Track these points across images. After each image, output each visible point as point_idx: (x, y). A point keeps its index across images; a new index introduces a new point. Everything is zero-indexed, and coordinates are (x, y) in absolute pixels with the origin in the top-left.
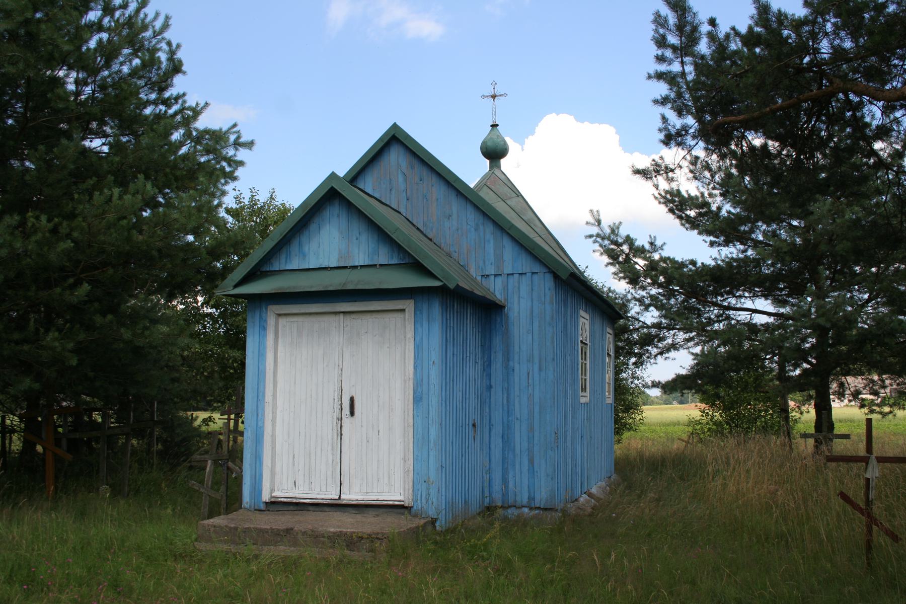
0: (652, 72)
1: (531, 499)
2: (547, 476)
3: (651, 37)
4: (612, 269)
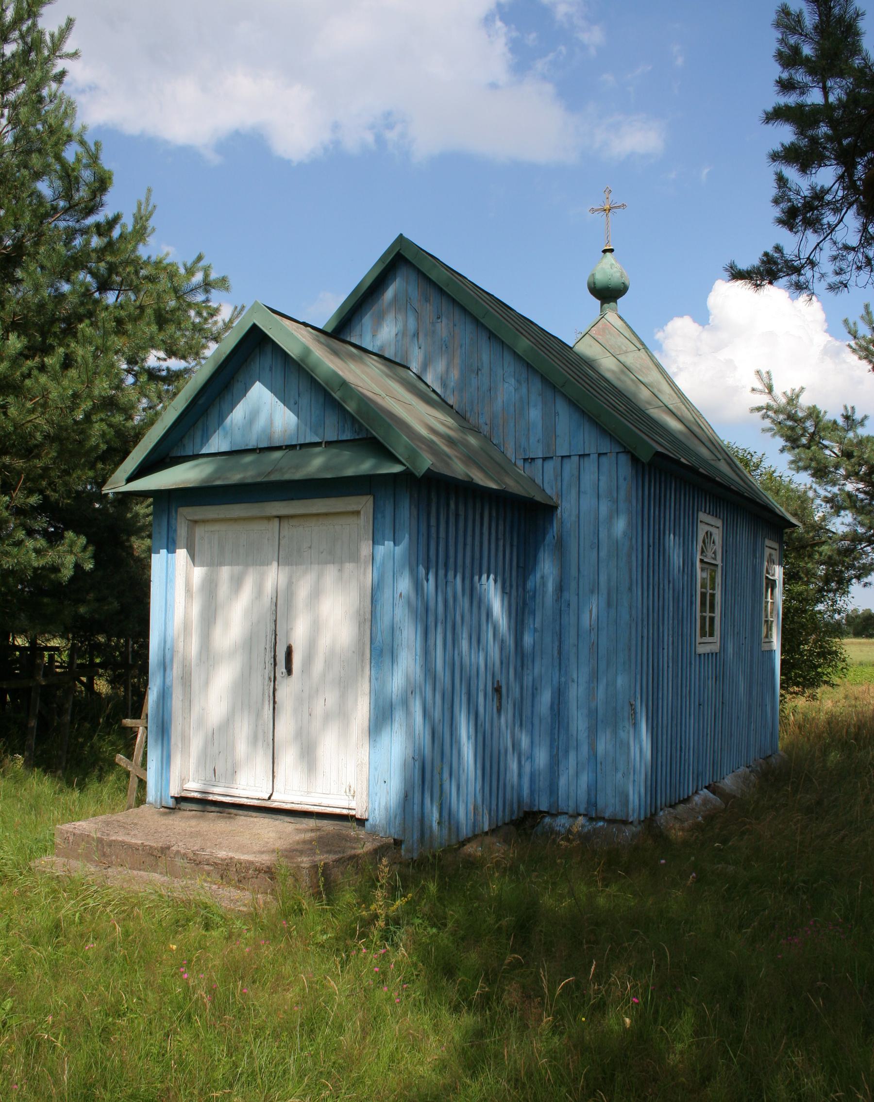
0: (770, 109)
1: (592, 803)
3: (773, 52)
4: (788, 456)
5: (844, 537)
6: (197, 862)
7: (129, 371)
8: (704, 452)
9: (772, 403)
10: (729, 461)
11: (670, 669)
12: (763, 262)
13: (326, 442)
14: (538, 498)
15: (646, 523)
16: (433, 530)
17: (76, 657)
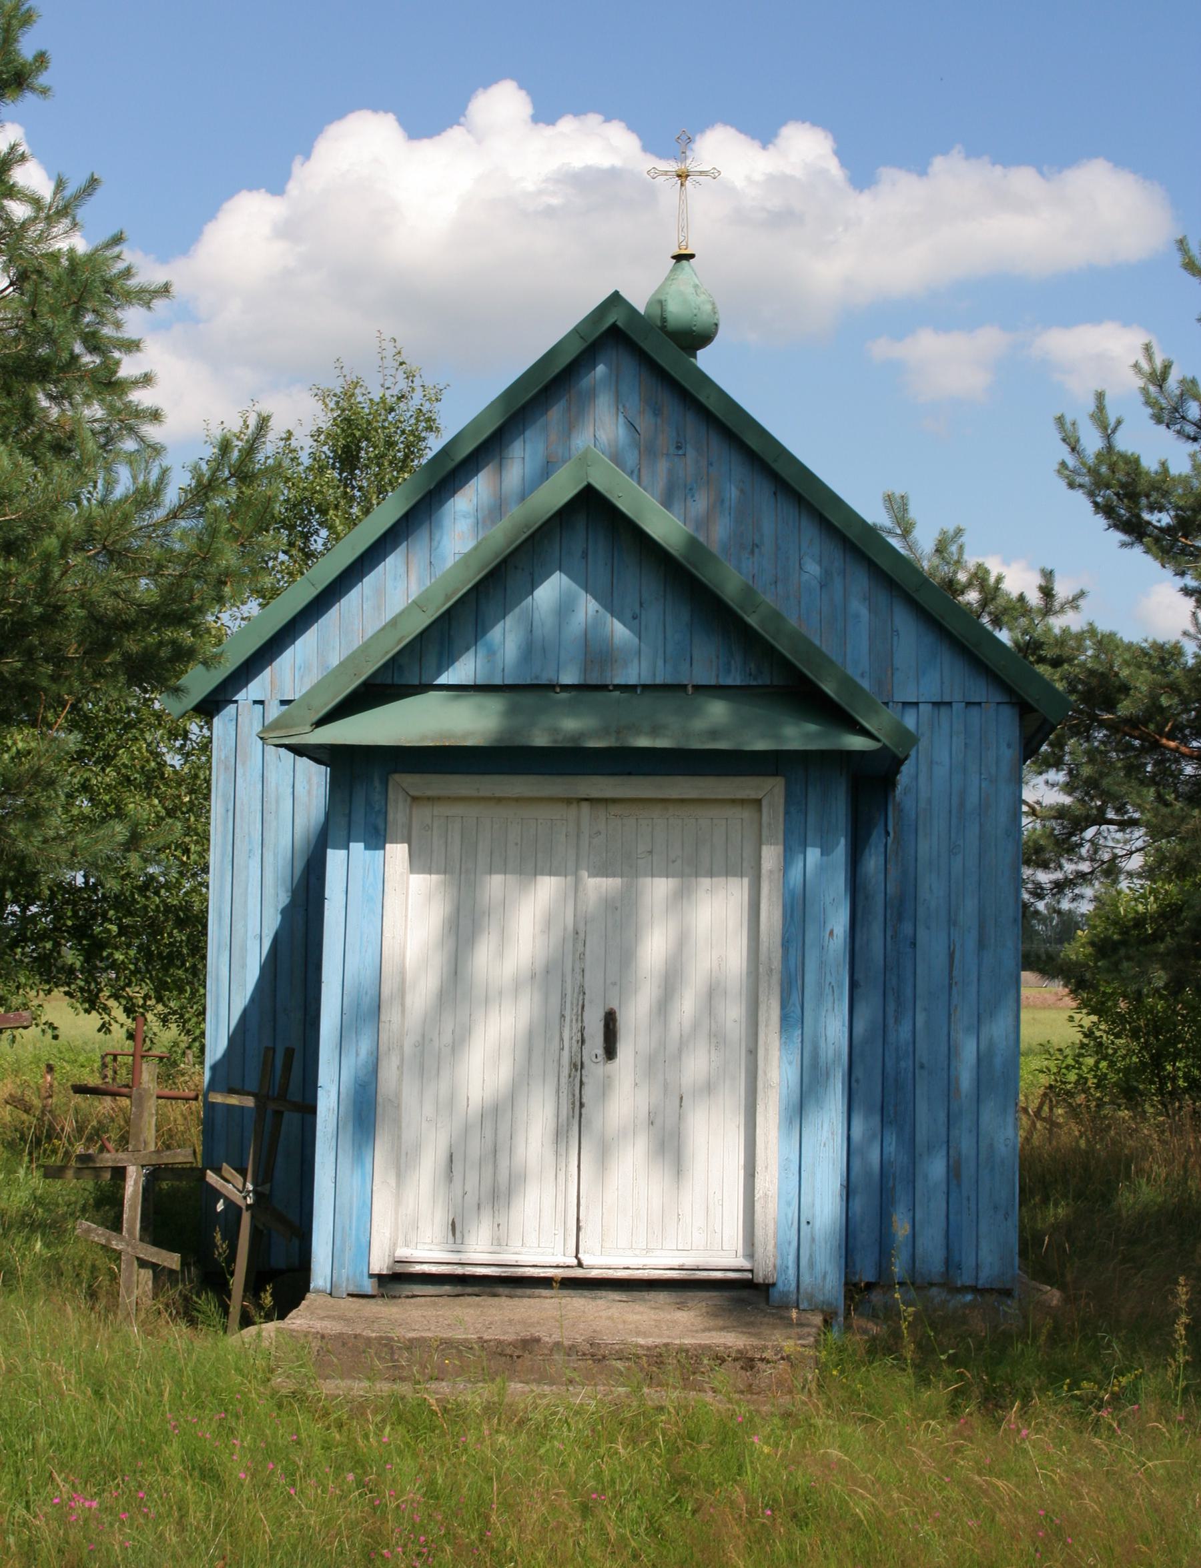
2: (996, 1208)
13: (694, 686)
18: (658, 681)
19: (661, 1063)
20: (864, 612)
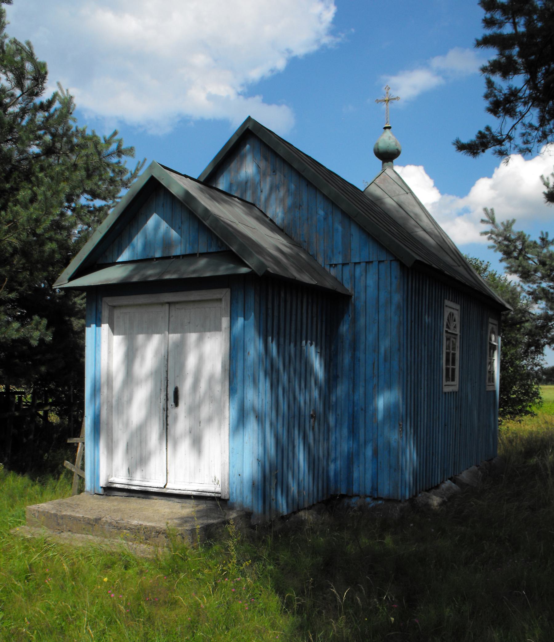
0: (480, 38)
1: (375, 488)
2: (390, 467)
5: (539, 318)
6: (118, 528)
7: (69, 207)
8: (449, 260)
9: (494, 229)
10: (466, 267)
11: (426, 402)
12: (478, 137)
14: (339, 290)
15: (409, 306)
16: (270, 311)
17: (36, 398)
18: (187, 253)
19: (193, 410)
20: (340, 228)
